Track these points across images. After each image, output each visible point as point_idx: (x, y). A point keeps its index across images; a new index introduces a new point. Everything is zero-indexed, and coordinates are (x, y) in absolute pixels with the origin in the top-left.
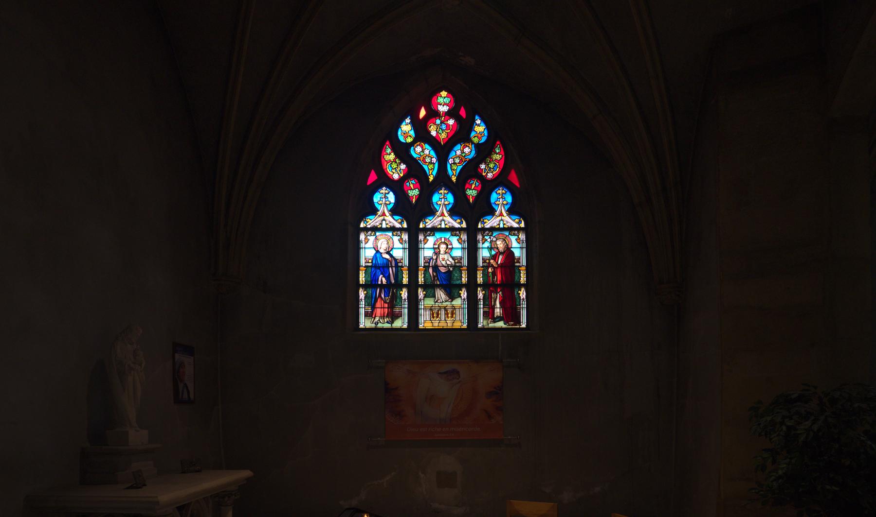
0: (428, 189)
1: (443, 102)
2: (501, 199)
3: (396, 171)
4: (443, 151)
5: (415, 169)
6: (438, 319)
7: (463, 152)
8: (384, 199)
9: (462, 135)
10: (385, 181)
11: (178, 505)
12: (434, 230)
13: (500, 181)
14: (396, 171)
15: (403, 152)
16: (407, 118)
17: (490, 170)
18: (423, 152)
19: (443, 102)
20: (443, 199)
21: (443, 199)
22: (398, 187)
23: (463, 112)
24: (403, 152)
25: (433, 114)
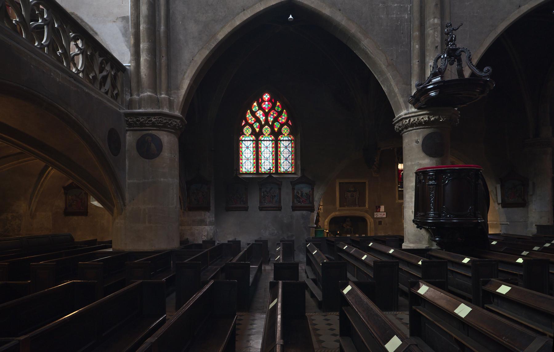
0: (261, 127)
1: (266, 97)
2: (285, 130)
3: (251, 120)
4: (266, 115)
5: (258, 120)
6: (307, 201)
7: (273, 114)
8: (247, 130)
9: (272, 108)
10: (247, 123)
11: (114, 102)
12: (498, 301)
13: (286, 123)
14: (251, 120)
15: (253, 114)
16: (255, 102)
17: (283, 119)
18: (260, 114)
19: (266, 97)
20: (267, 130)
21: (267, 130)
22: (251, 125)
23: (273, 101)
24: (253, 114)
25: (263, 101)
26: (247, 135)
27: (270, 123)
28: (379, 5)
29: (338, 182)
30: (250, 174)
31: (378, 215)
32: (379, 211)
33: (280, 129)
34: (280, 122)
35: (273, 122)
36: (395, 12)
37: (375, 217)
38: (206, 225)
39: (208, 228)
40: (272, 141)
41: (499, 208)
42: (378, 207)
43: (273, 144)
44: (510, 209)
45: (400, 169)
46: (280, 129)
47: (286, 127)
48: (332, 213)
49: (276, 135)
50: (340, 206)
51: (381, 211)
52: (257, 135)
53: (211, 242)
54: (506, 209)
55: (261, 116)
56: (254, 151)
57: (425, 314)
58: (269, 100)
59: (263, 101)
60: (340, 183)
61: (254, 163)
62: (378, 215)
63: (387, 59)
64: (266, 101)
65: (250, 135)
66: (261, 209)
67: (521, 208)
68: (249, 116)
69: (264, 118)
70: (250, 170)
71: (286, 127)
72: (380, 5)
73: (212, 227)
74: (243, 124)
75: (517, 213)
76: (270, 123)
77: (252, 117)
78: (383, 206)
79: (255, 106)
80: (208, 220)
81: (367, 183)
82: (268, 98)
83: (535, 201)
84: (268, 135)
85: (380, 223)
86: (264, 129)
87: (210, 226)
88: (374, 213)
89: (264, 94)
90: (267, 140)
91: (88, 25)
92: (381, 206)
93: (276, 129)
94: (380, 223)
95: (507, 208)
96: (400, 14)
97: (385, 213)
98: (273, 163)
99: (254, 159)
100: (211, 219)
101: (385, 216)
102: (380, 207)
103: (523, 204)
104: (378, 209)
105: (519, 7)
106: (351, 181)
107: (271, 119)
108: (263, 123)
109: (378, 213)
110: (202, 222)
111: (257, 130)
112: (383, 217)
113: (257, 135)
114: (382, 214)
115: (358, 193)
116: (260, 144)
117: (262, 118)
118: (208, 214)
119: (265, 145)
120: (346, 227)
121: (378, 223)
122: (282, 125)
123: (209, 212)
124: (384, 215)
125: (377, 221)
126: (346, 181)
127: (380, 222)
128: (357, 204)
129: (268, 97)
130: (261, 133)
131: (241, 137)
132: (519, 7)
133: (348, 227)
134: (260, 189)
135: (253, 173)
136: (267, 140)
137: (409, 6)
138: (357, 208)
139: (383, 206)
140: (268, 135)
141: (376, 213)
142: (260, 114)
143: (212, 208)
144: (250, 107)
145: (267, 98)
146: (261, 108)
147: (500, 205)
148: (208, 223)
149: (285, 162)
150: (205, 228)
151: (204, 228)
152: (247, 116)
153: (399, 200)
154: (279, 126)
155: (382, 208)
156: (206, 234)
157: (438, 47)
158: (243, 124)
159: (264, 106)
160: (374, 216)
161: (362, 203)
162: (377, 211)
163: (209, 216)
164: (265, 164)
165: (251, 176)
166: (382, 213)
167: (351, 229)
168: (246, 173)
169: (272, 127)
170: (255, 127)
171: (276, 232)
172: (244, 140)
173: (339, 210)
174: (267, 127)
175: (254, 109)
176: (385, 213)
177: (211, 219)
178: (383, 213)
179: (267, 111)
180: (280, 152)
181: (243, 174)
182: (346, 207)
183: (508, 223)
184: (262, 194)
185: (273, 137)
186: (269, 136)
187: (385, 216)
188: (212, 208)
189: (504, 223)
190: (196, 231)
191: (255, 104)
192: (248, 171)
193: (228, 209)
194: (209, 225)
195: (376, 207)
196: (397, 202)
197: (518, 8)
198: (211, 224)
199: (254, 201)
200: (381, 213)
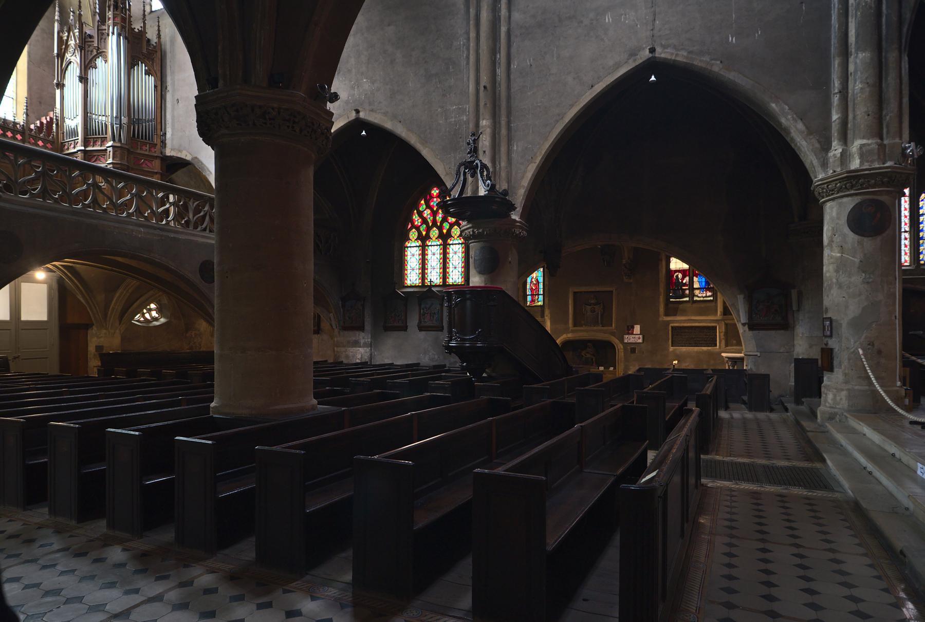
0: (428, 229)
4: (434, 214)
5: (424, 221)
8: (413, 234)
10: (414, 226)
15: (420, 214)
18: (427, 213)
20: (435, 232)
21: (435, 232)
22: (417, 228)
24: (420, 214)
25: (432, 197)
26: (413, 240)
27: (439, 224)
28: (437, 110)
29: (571, 290)
30: (415, 286)
31: (629, 339)
32: (632, 334)
33: (449, 231)
34: (450, 221)
35: (442, 222)
36: (453, 115)
37: (626, 341)
38: (360, 347)
39: (361, 350)
40: (462, 244)
41: (745, 331)
42: (630, 327)
43: (463, 248)
44: (762, 333)
45: (673, 269)
46: (449, 231)
47: (456, 227)
48: (562, 336)
49: (445, 238)
50: (575, 325)
51: (634, 333)
52: (424, 239)
53: (364, 364)
54: (756, 332)
55: (429, 216)
56: (420, 259)
57: (537, 453)
58: (438, 196)
59: (432, 197)
60: (575, 293)
61: (420, 274)
62: (629, 339)
63: (445, 168)
64: (434, 198)
65: (416, 240)
66: (421, 328)
67: (782, 331)
68: (416, 217)
69: (432, 218)
70: (415, 283)
71: (456, 227)
72: (439, 110)
73: (368, 350)
74: (409, 226)
75: (775, 338)
76: (439, 224)
77: (419, 218)
78: (639, 326)
79: (422, 204)
80: (362, 341)
81: (614, 291)
82: (437, 193)
83: (802, 320)
84: (458, 237)
85: (633, 351)
86: (431, 232)
87: (365, 348)
88: (625, 336)
89: (432, 189)
90: (434, 246)
91: (206, 166)
92: (635, 326)
93: (445, 231)
94: (633, 351)
95: (758, 331)
96: (459, 116)
97: (641, 336)
98: (441, 273)
99: (420, 269)
100: (366, 340)
101: (640, 341)
102: (633, 327)
103: (785, 325)
104: (630, 331)
105: (592, 86)
106: (593, 289)
107: (439, 218)
108: (430, 224)
109: (630, 336)
110: (356, 344)
111: (424, 233)
112: (638, 342)
113: (424, 239)
114: (636, 336)
115: (602, 307)
116: (449, 249)
117: (430, 219)
118: (362, 334)
119: (433, 251)
120: (586, 355)
121: (630, 350)
122: (452, 225)
123: (363, 332)
124: (639, 338)
125: (629, 347)
126: (583, 289)
127: (632, 349)
128: (599, 322)
129: (437, 192)
130: (428, 237)
131: (407, 243)
132: (592, 86)
133: (588, 356)
134: (420, 305)
135: (418, 286)
136: (434, 246)
137: (467, 106)
138: (600, 328)
139: (639, 326)
140: (458, 237)
141: (626, 336)
142: (427, 213)
143: (368, 326)
144: (416, 206)
145: (435, 194)
146: (428, 206)
147: (747, 326)
148: (362, 344)
149: (454, 272)
150: (359, 350)
151: (359, 350)
152: (414, 217)
153: (664, 317)
154: (448, 227)
155: (637, 329)
156: (359, 356)
157: (486, 152)
158: (409, 226)
159: (432, 204)
160: (623, 341)
161: (605, 320)
162: (628, 334)
163: (364, 337)
164: (432, 274)
165: (416, 290)
166: (636, 336)
167: (592, 359)
168: (411, 287)
169: (440, 228)
170: (421, 230)
171: (436, 357)
172: (409, 247)
173: (573, 331)
174: (435, 228)
175: (421, 209)
176: (641, 336)
177: (366, 340)
178: (638, 336)
179: (435, 209)
180: (448, 258)
181: (408, 287)
182: (584, 326)
183: (759, 354)
184: (422, 311)
185: (441, 241)
186: (437, 240)
187: (640, 341)
188: (368, 326)
189: (751, 353)
190: (351, 353)
191: (423, 202)
192: (413, 283)
193: (387, 329)
194: (363, 347)
195: (628, 327)
196: (661, 319)
197: (591, 88)
198: (365, 345)
199: (413, 321)
200: (634, 336)
